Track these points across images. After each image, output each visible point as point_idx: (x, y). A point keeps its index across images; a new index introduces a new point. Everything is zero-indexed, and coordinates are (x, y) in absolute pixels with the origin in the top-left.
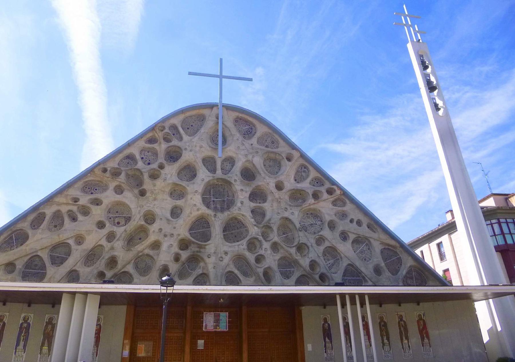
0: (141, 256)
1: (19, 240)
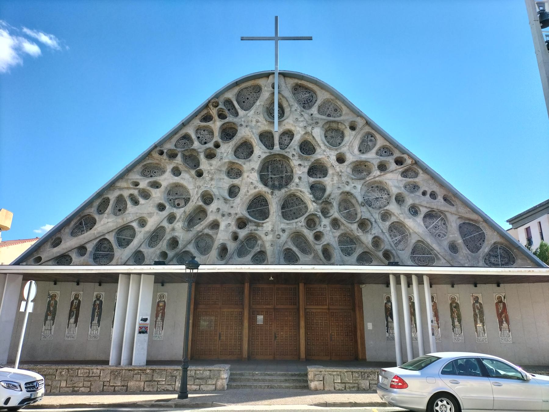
0: (201, 235)
1: (88, 225)
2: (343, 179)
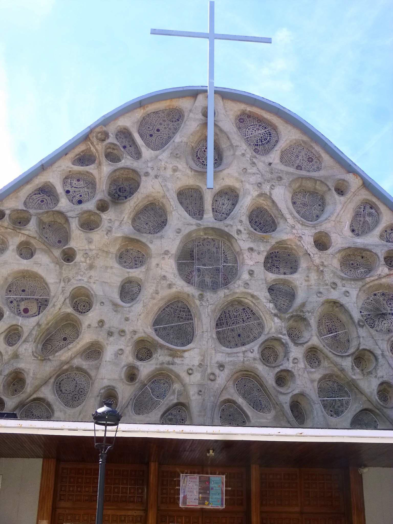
0: (67, 370)
2: (326, 278)
